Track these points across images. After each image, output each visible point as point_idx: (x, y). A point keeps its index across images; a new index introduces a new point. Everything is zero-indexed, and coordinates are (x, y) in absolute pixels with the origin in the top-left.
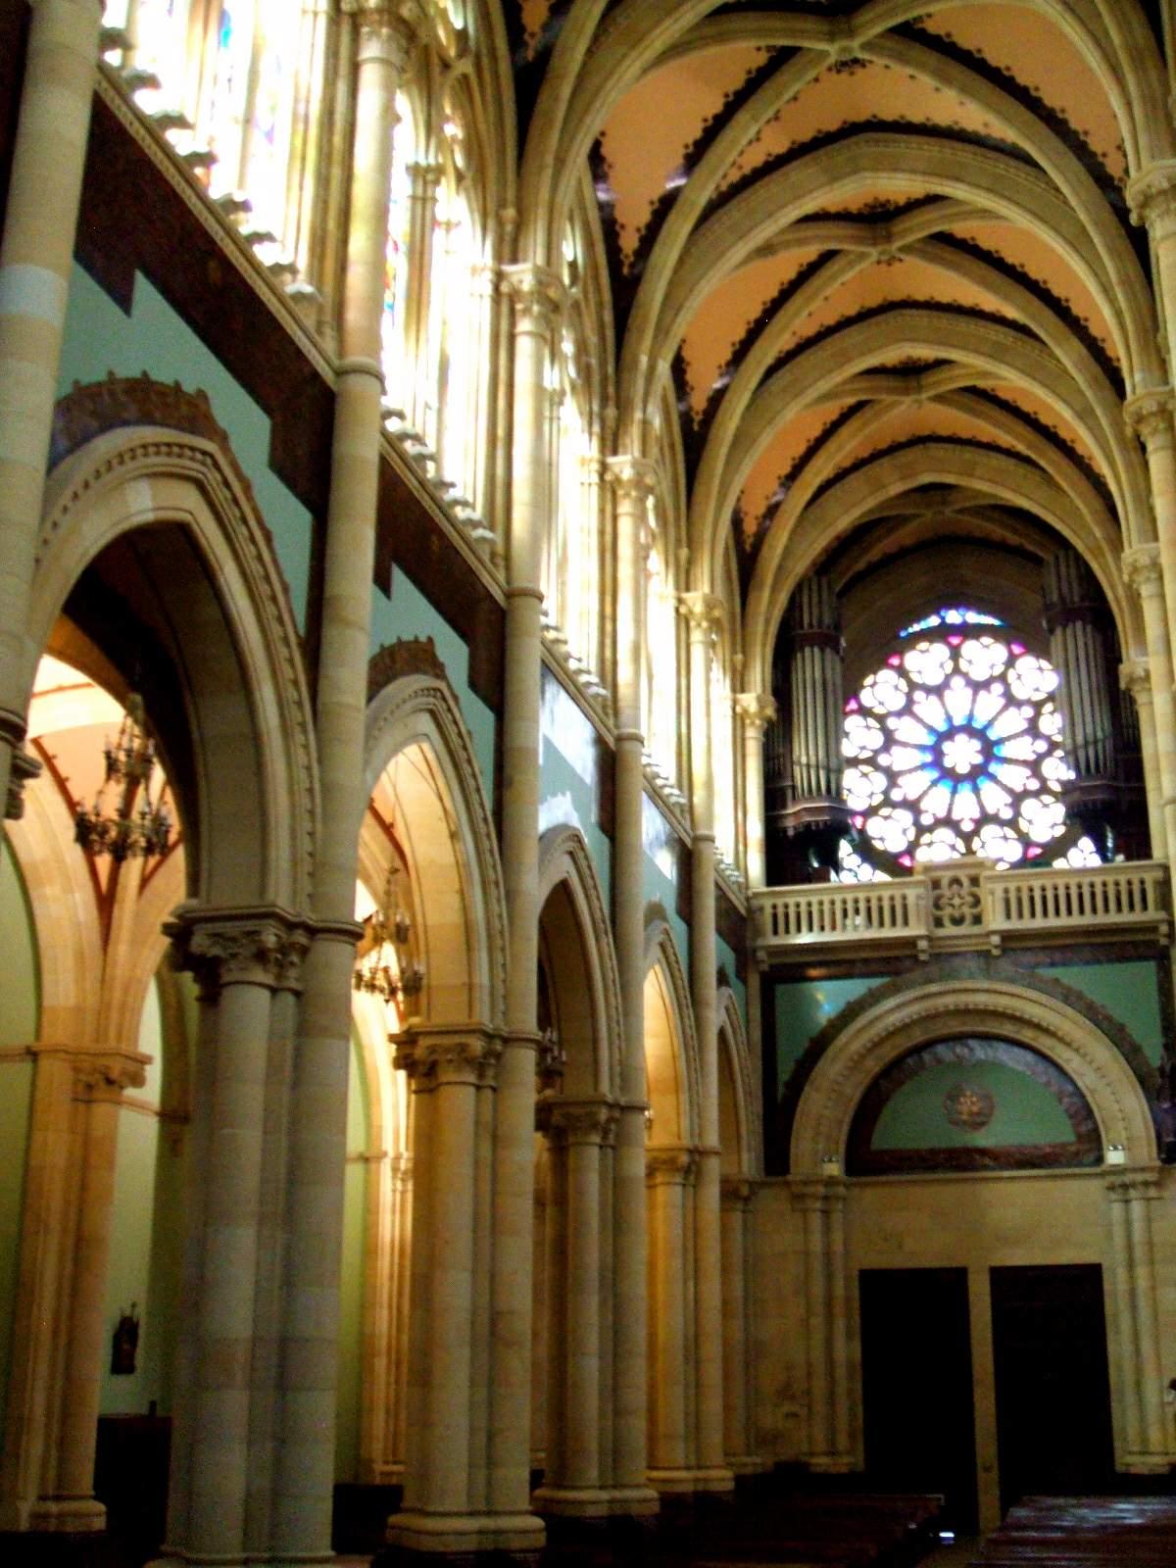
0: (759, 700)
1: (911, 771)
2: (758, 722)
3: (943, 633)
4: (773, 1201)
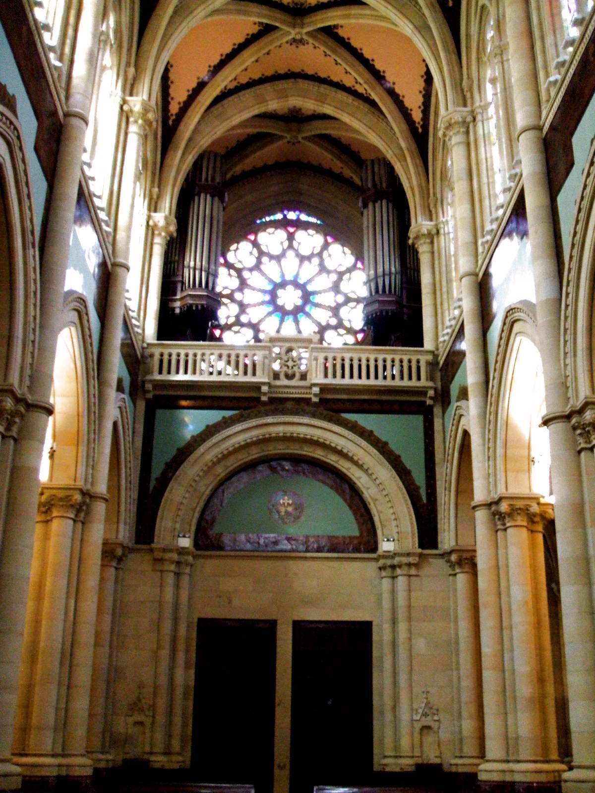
0: (166, 218)
1: (255, 305)
2: (163, 234)
3: (285, 224)
4: (139, 563)
